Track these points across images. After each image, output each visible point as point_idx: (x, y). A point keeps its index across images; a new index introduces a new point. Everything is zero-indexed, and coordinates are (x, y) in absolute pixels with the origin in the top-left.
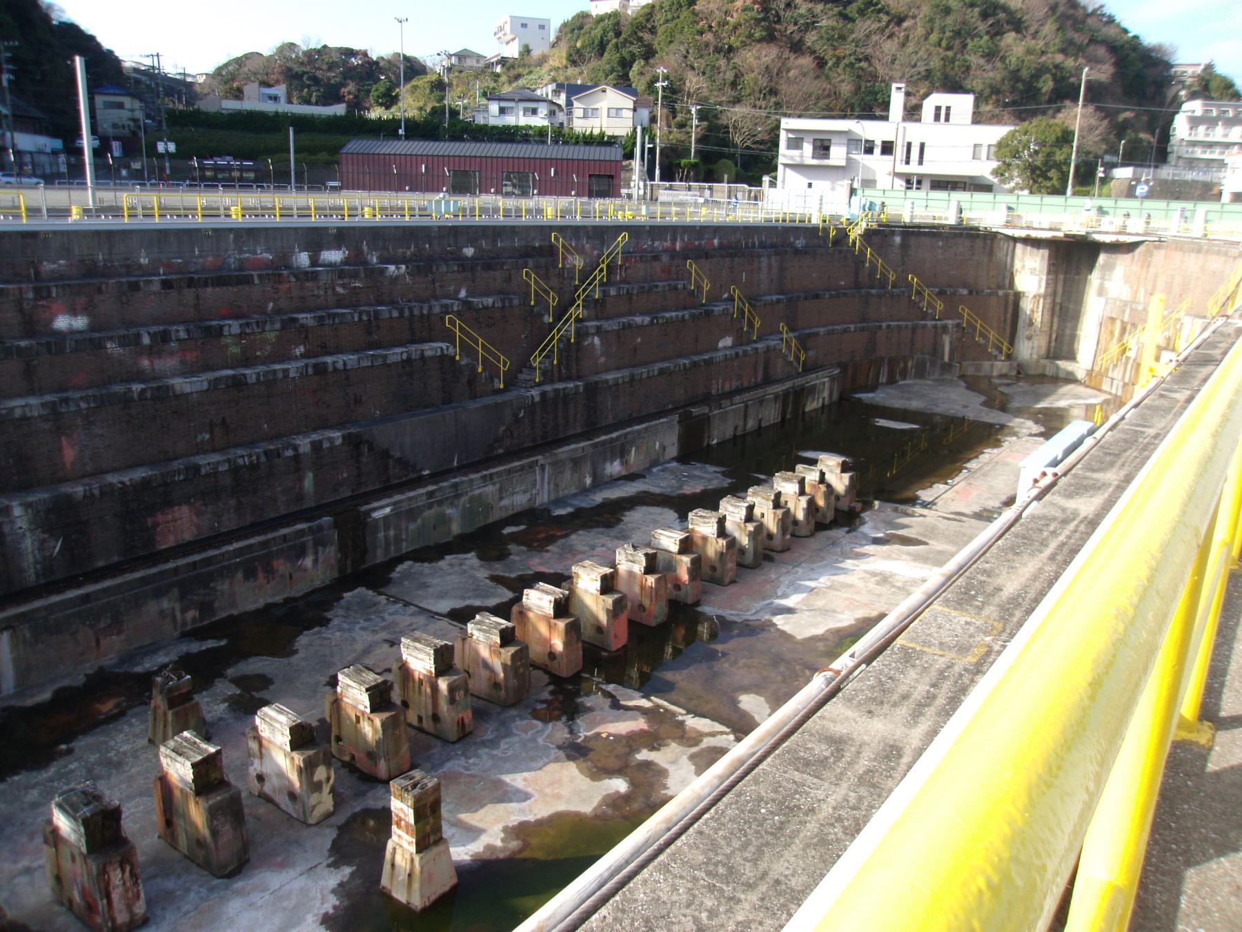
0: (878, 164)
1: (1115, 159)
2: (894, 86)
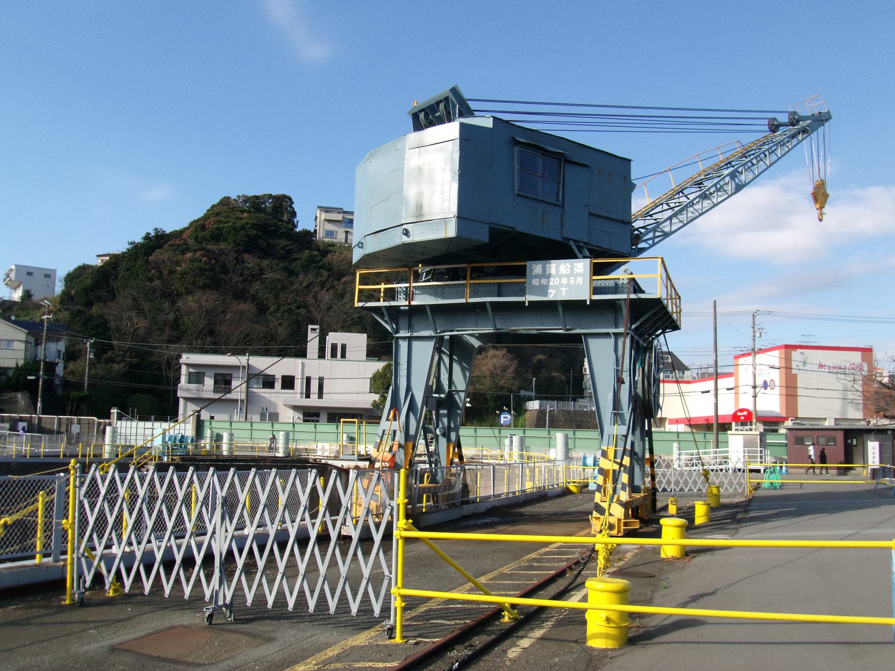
0: (277, 397)
1: (527, 393)
2: (310, 327)
